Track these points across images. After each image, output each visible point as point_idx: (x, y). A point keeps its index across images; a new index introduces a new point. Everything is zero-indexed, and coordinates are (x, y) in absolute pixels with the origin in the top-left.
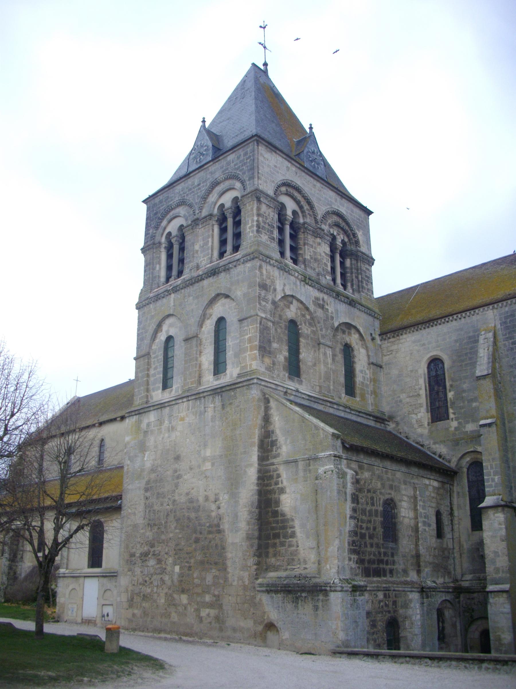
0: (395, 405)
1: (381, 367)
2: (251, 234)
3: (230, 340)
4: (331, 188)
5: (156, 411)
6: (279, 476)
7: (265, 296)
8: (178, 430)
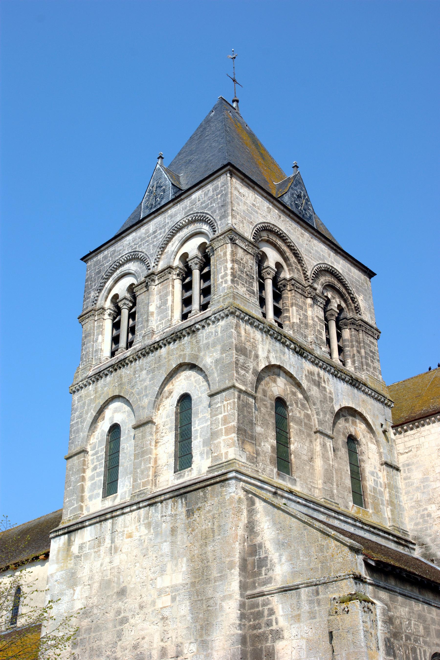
0: (421, 521)
1: (398, 469)
2: (224, 285)
3: (197, 422)
4: (323, 239)
5: (93, 526)
6: (272, 612)
7: (244, 363)
8: (124, 551)
